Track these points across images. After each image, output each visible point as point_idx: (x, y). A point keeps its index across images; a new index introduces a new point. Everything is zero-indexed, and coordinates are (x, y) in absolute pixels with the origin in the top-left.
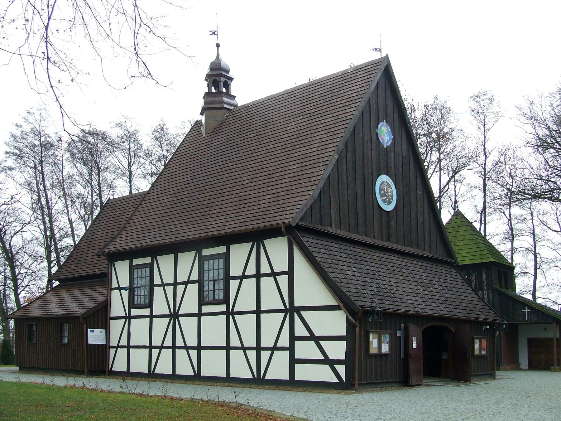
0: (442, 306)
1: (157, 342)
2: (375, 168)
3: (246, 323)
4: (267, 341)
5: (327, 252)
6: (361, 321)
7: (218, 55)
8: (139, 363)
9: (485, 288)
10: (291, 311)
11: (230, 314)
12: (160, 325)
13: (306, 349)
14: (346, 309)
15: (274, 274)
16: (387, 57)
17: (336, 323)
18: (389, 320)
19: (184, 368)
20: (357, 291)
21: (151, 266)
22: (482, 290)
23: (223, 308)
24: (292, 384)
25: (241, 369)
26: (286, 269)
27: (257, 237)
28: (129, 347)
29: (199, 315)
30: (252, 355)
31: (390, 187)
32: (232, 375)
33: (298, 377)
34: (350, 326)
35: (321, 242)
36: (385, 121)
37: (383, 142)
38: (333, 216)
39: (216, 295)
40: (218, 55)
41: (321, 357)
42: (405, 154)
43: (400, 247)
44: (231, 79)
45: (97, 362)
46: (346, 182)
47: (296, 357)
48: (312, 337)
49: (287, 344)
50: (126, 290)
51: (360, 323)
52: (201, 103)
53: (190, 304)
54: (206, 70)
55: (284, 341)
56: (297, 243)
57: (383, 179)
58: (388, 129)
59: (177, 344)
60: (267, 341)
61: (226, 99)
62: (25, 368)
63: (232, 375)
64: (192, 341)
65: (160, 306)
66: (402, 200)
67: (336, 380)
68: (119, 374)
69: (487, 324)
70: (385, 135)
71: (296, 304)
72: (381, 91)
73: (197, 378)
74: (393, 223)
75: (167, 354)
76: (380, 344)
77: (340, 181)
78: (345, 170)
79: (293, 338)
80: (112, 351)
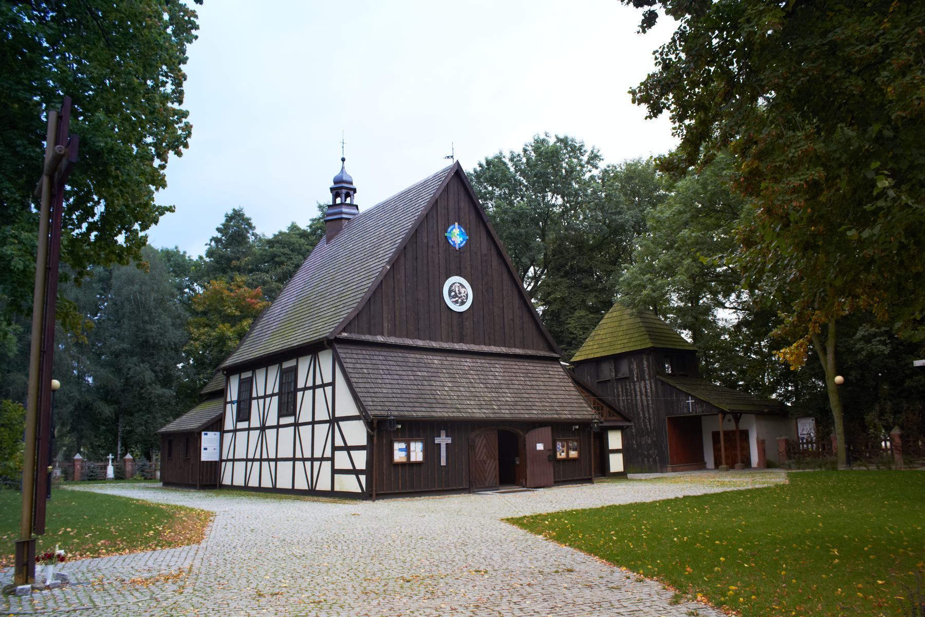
6: (382, 431)
7: (343, 168)
9: (647, 377)
13: (342, 460)
17: (356, 433)
18: (413, 428)
26: (331, 381)
31: (463, 287)
34: (370, 437)
38: (386, 325)
40: (343, 168)
42: (484, 251)
47: (336, 468)
49: (330, 456)
55: (328, 454)
59: (297, 456)
68: (232, 488)
70: (457, 236)
71: (337, 415)
78: (403, 278)
79: (334, 449)
80: (223, 464)
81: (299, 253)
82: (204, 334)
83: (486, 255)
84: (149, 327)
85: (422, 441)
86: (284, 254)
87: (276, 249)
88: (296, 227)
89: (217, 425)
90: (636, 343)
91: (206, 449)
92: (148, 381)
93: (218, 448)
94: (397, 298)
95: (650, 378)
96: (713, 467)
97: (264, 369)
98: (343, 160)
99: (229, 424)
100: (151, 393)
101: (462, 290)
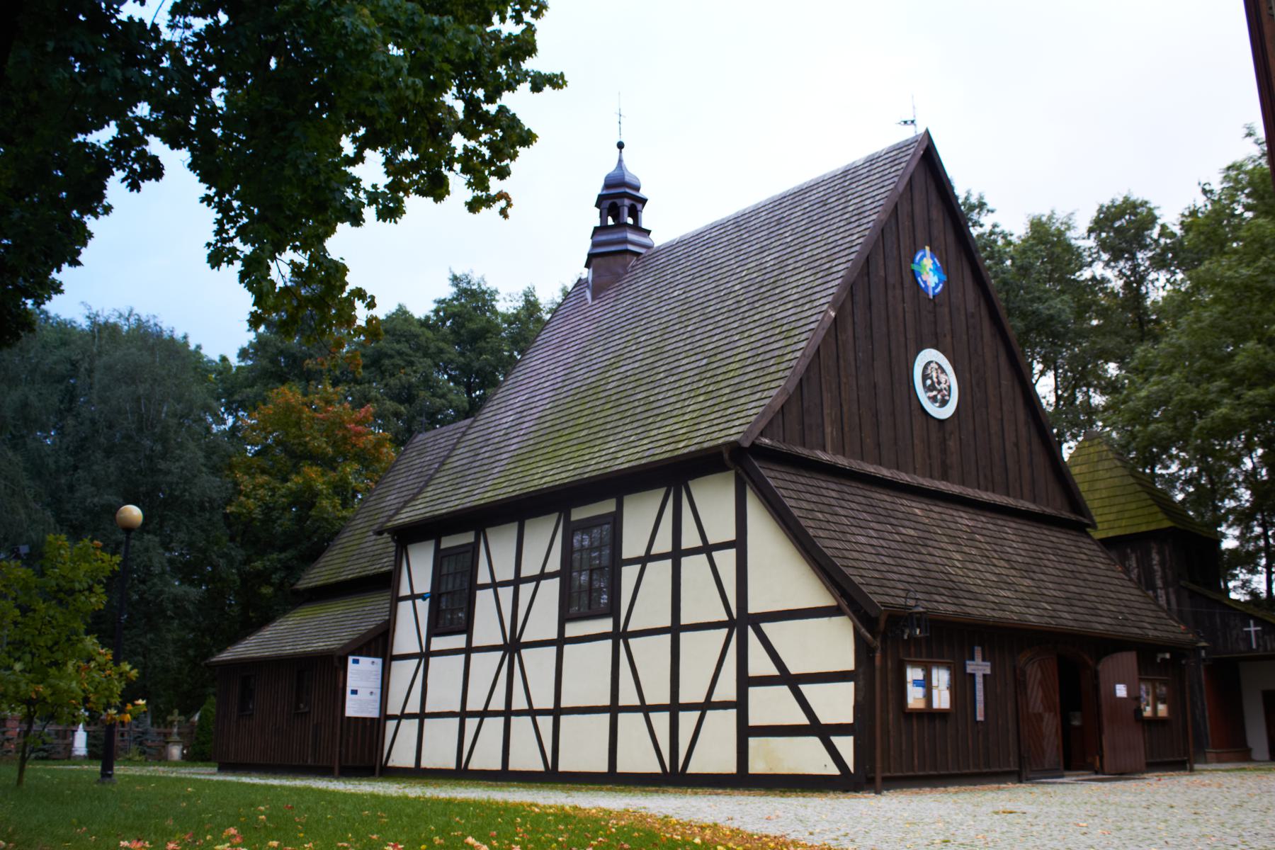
0: (1065, 608)
1: (475, 704)
2: (911, 335)
3: (651, 655)
4: (692, 691)
5: (814, 499)
6: (889, 641)
7: (620, 161)
8: (440, 753)
9: (1159, 583)
10: (742, 623)
11: (620, 636)
12: (485, 665)
13: (771, 705)
14: (854, 612)
15: (707, 549)
16: (927, 133)
17: (829, 644)
18: (947, 639)
19: (526, 757)
20: (876, 575)
21: (473, 550)
22: (1154, 588)
23: (606, 625)
24: (742, 780)
25: (638, 755)
26: (731, 535)
27: (674, 476)
28: (422, 716)
29: (561, 642)
30: (661, 721)
31: (943, 371)
32: (620, 769)
33: (757, 766)
35: (802, 480)
36: (927, 248)
37: (927, 286)
38: (828, 430)
39: (591, 590)
40: (620, 161)
41: (803, 720)
42: (971, 307)
43: (970, 492)
44: (643, 201)
45: (362, 750)
46: (853, 363)
48: (786, 678)
50: (424, 599)
51: (884, 641)
52: (585, 246)
53: (543, 622)
54: (598, 188)
55: (727, 689)
56: (753, 481)
57: (929, 355)
58: (934, 263)
60: (692, 691)
61: (631, 236)
62: (225, 767)
63: (620, 769)
64: (543, 699)
65: (487, 628)
66: (969, 398)
67: (834, 770)
69: (1164, 649)
70: (929, 272)
71: (753, 608)
72: (919, 196)
73: (551, 776)
74: (952, 444)
75: (494, 726)
76: (930, 689)
77: (841, 362)
78: (851, 341)
79: (745, 681)
80: (391, 725)
81: (426, 355)
82: (262, 486)
83: (973, 315)
84: (163, 465)
85: (949, 668)
86: (400, 353)
87: (384, 344)
88: (405, 313)
89: (378, 644)
90: (1136, 521)
91: (354, 692)
92: (156, 569)
93: (378, 692)
94: (844, 380)
95: (1166, 585)
96: (1267, 757)
97: (512, 529)
98: (621, 146)
99: (406, 638)
100: (161, 592)
101: (943, 378)
